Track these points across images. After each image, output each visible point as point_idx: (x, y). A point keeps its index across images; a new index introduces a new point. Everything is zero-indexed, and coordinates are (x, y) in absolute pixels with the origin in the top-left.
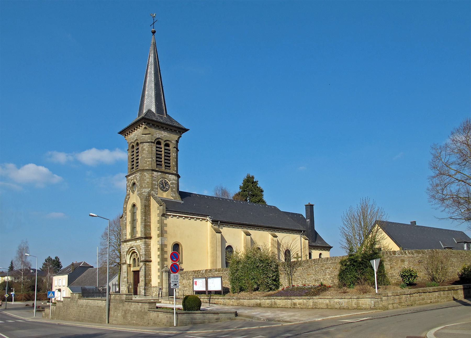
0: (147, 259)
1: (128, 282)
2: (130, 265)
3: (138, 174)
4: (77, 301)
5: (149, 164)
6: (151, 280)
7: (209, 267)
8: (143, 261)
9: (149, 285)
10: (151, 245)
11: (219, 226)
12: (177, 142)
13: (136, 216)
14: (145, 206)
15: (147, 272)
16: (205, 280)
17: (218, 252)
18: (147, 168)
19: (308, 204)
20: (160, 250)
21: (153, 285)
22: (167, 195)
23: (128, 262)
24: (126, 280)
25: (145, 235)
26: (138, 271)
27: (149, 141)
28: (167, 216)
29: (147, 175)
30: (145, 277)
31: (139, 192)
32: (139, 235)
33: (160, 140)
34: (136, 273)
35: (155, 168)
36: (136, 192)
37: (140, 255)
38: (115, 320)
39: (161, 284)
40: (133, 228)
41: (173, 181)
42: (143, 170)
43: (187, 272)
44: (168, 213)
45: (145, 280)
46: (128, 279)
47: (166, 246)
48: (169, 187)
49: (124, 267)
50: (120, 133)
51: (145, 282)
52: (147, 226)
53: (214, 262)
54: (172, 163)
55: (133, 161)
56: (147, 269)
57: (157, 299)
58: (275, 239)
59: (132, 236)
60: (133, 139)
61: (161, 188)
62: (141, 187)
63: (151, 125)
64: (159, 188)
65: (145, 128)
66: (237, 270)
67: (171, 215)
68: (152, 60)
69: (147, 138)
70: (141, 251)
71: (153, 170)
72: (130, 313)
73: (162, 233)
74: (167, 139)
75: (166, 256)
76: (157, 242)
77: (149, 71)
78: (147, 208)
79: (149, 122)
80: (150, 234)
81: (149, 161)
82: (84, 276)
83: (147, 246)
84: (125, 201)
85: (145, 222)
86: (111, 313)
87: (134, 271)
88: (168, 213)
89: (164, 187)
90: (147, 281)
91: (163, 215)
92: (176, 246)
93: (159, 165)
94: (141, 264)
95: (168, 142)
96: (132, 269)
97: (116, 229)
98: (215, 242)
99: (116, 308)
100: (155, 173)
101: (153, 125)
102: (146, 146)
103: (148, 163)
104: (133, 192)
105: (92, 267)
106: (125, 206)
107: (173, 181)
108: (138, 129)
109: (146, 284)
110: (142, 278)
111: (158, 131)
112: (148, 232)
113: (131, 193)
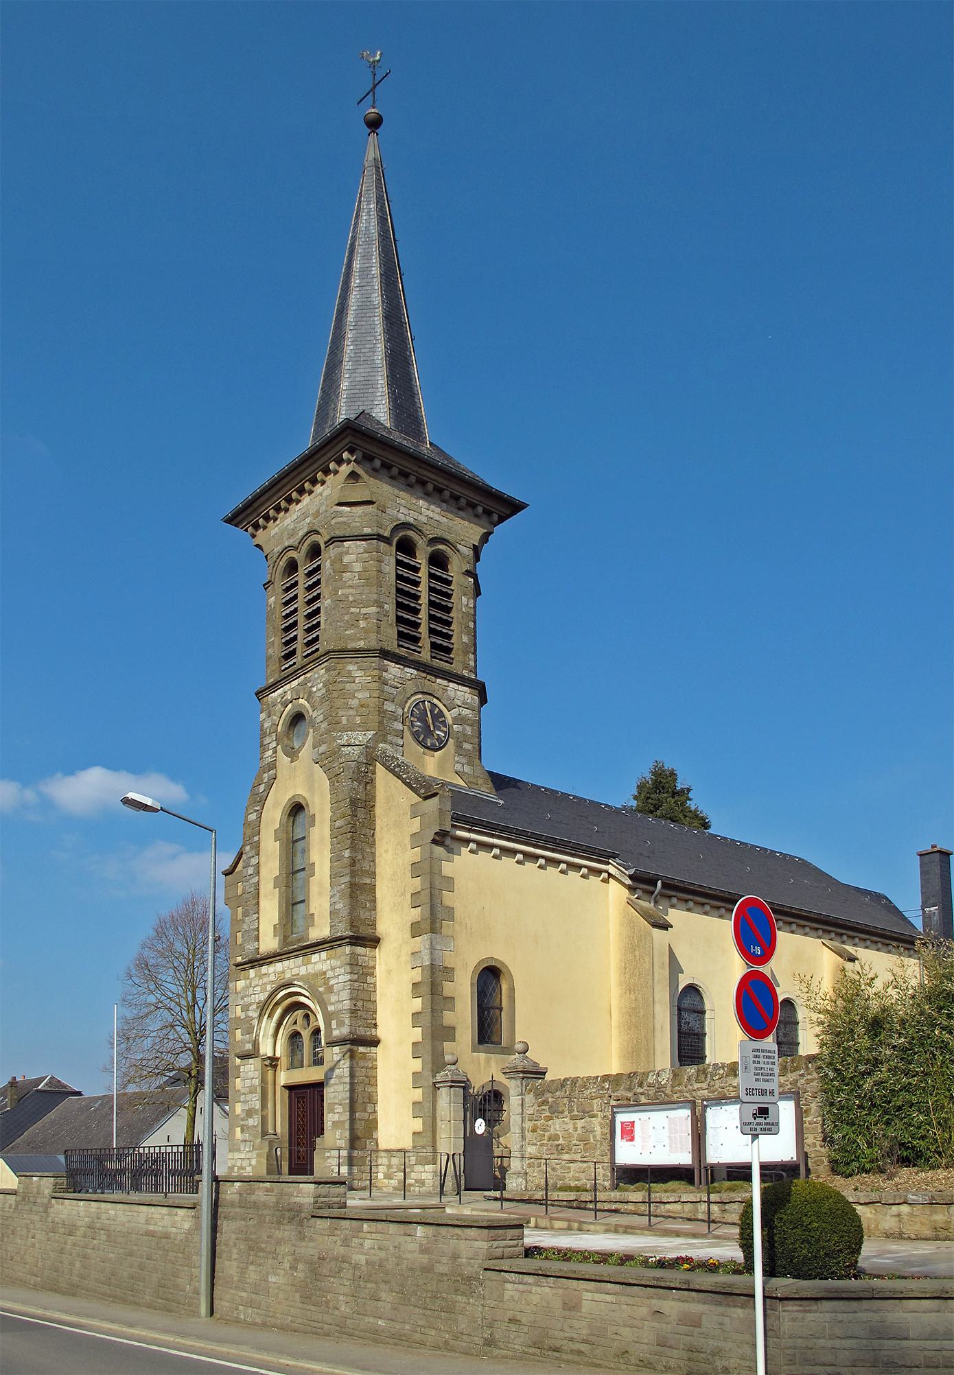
0: (362, 1031)
1: (264, 1133)
2: (273, 1062)
3: (318, 676)
4: (46, 1207)
5: (366, 631)
6: (376, 1121)
7: (615, 1068)
8: (341, 1042)
9: (370, 1145)
10: (378, 972)
11: (656, 902)
12: (477, 550)
13: (305, 851)
14: (354, 803)
15: (359, 1088)
16: (685, 1113)
17: (658, 1008)
18: (361, 644)
19: (930, 849)
20: (426, 989)
21: (382, 1146)
22: (441, 766)
23: (266, 1049)
24: (254, 1121)
25: (352, 926)
26: (319, 1086)
27: (367, 531)
28: (454, 845)
29: (359, 674)
30: (352, 1111)
31: (323, 748)
32: (320, 930)
33: (411, 533)
34: (306, 1101)
35: (392, 644)
36: (306, 752)
37: (328, 1017)
38: (250, 1304)
39: (426, 1140)
40: (293, 903)
41: (465, 712)
42: (343, 653)
43: (570, 1085)
44: (459, 833)
45: (352, 1120)
46: (264, 1120)
47: (449, 972)
48: (448, 735)
49: (247, 1075)
50: (234, 519)
51: (352, 1129)
52: (358, 888)
53: (638, 1047)
54: (460, 638)
55: (295, 624)
56: (360, 1073)
57: (435, 1201)
58: (849, 965)
59: (285, 940)
60: (291, 536)
61: (416, 735)
62: (334, 724)
63: (377, 463)
64: (407, 734)
65: (353, 476)
66: (876, 1063)
67: (468, 841)
68: (368, 223)
69: (358, 518)
70: (333, 998)
71: (385, 654)
72: (348, 1273)
73: (434, 917)
74: (439, 533)
75: (448, 1018)
76: (405, 957)
77: (356, 266)
78: (361, 814)
79: (373, 449)
80: (373, 925)
81: (366, 617)
82: (53, 1122)
83: (362, 974)
84: (254, 794)
85: (353, 874)
86: (228, 1267)
87: (290, 1088)
88: (459, 833)
89: (429, 733)
90: (360, 1126)
91: (441, 838)
92: (490, 975)
93: (408, 636)
94: (334, 1054)
95: (441, 547)
96: (284, 1078)
97: (179, 946)
98: (647, 965)
99: (254, 1247)
100: (394, 670)
101: (387, 466)
102: (354, 553)
103: (362, 624)
104: (292, 753)
105: (79, 1094)
106: (253, 817)
107: (465, 712)
108: (318, 489)
109: (354, 1141)
110: (335, 1115)
111: (404, 497)
112: (364, 915)
113: (283, 760)
